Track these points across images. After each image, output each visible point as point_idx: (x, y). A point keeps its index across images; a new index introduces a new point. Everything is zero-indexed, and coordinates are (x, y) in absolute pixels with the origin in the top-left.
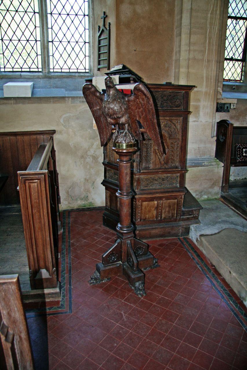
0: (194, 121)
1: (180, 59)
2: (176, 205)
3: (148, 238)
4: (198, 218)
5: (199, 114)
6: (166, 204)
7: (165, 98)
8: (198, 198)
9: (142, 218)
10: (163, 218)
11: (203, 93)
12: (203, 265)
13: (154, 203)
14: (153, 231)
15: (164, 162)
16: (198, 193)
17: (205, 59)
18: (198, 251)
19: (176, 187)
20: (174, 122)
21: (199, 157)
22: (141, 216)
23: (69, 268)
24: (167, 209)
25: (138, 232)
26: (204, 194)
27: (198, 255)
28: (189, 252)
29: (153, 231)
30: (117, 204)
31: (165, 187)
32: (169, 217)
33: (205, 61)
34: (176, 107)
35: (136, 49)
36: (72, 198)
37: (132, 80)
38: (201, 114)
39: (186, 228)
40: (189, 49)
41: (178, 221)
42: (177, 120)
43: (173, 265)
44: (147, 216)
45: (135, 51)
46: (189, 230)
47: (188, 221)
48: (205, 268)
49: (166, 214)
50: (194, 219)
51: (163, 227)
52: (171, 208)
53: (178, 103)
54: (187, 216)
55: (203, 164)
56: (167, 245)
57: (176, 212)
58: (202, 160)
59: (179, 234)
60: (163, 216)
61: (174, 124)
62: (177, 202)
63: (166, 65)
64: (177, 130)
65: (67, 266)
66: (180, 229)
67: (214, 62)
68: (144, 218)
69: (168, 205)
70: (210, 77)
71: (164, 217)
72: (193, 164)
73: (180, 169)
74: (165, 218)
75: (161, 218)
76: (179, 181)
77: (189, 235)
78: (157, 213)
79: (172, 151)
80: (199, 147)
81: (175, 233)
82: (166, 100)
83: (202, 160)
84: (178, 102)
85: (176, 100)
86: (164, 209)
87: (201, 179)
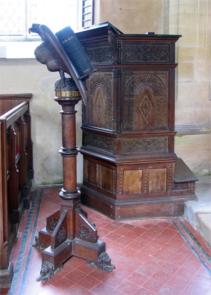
0: (188, 82)
1: (169, 15)
2: (166, 175)
3: (132, 216)
4: (194, 193)
5: (193, 73)
6: (153, 174)
7: (148, 50)
8: (197, 172)
9: (124, 190)
10: (150, 191)
11: (197, 50)
12: (200, 250)
13: (138, 172)
14: (138, 208)
15: (149, 122)
16: (196, 167)
17: (197, 13)
18: (194, 234)
19: (165, 152)
20: (159, 76)
21: (196, 122)
22: (123, 188)
23: (29, 249)
24: (155, 180)
25: (119, 208)
26: (204, 167)
27: (194, 238)
28: (183, 235)
29: (138, 208)
30: (95, 175)
31: (152, 153)
32: (158, 190)
33: (198, 15)
34: (161, 59)
35: (122, 7)
36: (48, 171)
37: (110, 30)
38: (196, 73)
39: (179, 205)
40: (179, 4)
41: (169, 196)
42: (163, 74)
43: (160, 249)
44: (131, 188)
45: (121, 9)
46: (184, 208)
47: (182, 196)
48: (203, 254)
49: (154, 187)
50: (189, 194)
51: (151, 203)
52: (160, 179)
53: (164, 55)
54: (180, 189)
55: (201, 131)
56: (155, 226)
57: (165, 184)
58: (200, 127)
59: (171, 213)
60: (150, 189)
61: (159, 78)
62: (167, 171)
63: (155, 23)
64: (164, 85)
65: (28, 247)
66: (172, 206)
67: (207, 15)
68: (127, 191)
69: (156, 174)
70: (204, 33)
71: (152, 190)
72: (189, 131)
73: (168, 131)
74: (152, 191)
75: (148, 191)
76: (168, 145)
77: (184, 214)
78: (143, 184)
79: (159, 110)
80: (195, 112)
81: (165, 212)
82: (149, 53)
83: (200, 127)
84: (163, 54)
85: (161, 52)
86: (151, 180)
87: (200, 149)
